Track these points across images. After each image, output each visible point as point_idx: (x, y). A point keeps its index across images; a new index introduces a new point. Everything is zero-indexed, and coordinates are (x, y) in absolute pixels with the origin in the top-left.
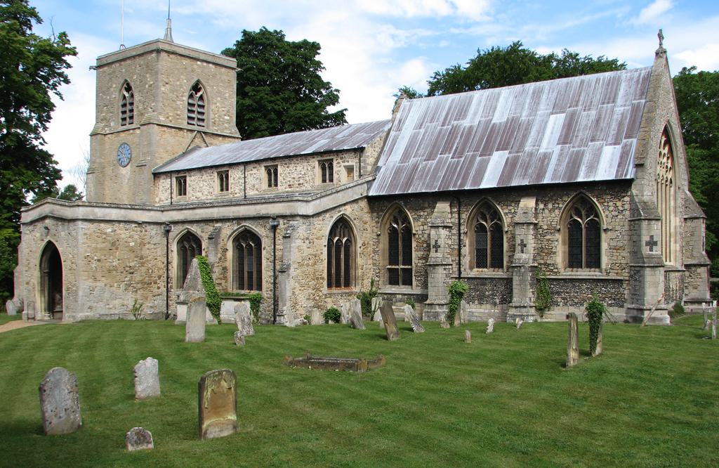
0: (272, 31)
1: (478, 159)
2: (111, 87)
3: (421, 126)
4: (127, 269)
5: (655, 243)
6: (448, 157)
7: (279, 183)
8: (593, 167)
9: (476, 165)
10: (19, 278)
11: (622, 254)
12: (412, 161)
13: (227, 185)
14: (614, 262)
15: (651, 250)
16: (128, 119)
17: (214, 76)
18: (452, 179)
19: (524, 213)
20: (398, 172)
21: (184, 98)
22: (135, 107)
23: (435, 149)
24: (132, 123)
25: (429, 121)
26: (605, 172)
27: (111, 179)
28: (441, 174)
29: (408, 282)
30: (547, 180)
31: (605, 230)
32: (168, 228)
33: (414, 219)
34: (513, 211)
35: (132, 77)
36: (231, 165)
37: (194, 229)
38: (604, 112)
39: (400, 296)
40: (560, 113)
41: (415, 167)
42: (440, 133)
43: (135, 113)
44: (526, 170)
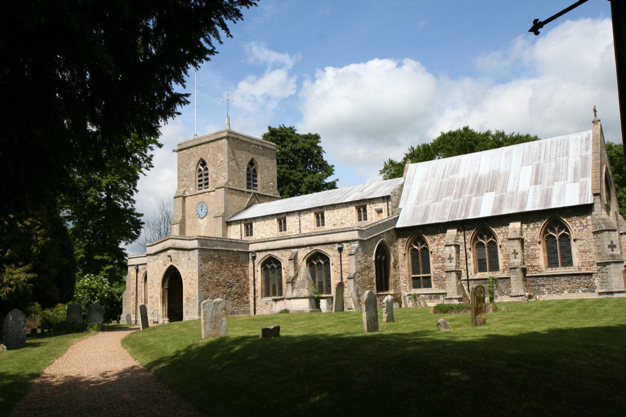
0: (278, 127)
1: (474, 199)
2: (190, 163)
3: (426, 179)
5: (615, 246)
6: (450, 199)
7: (326, 223)
9: (473, 204)
10: (127, 299)
11: (589, 255)
12: (425, 203)
14: (584, 261)
15: (612, 251)
16: (203, 185)
18: (457, 212)
19: (514, 232)
20: (415, 210)
21: (244, 170)
23: (440, 194)
24: (208, 188)
25: (432, 176)
27: (191, 228)
28: (448, 210)
29: (429, 285)
30: (529, 208)
31: (575, 240)
32: (254, 255)
33: (431, 241)
34: (504, 231)
35: (207, 156)
36: (288, 213)
37: (275, 254)
38: (561, 162)
39: (423, 296)
40: (528, 165)
41: (427, 208)
42: (441, 183)
43: (210, 181)
44: (511, 203)
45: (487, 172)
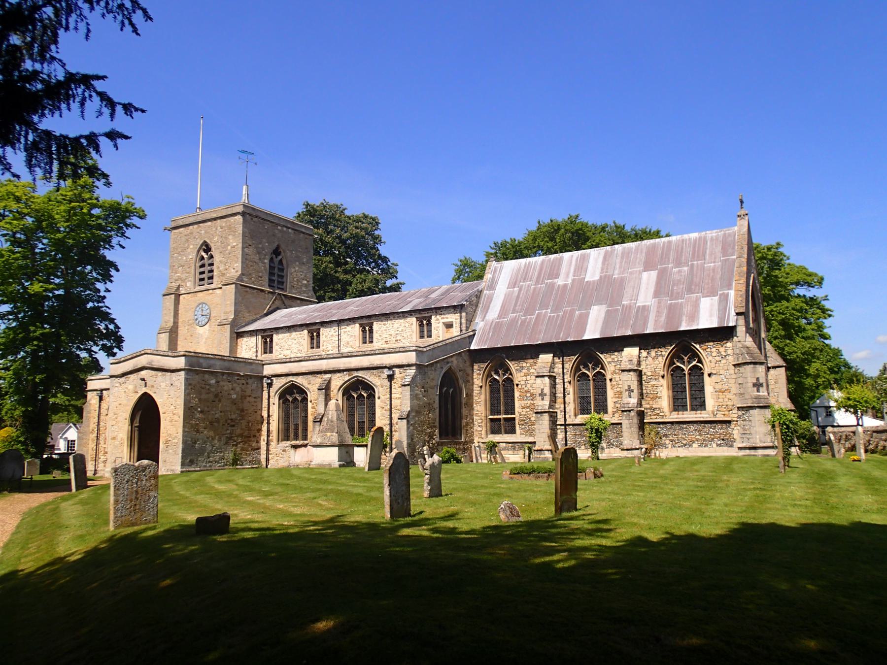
4: (229, 421)
5: (761, 385)
8: (694, 316)
13: (318, 342)
16: (206, 279)
17: (293, 241)
22: (214, 268)
26: (707, 320)
36: (323, 324)
37: (300, 381)
43: (215, 273)
45: (597, 278)
